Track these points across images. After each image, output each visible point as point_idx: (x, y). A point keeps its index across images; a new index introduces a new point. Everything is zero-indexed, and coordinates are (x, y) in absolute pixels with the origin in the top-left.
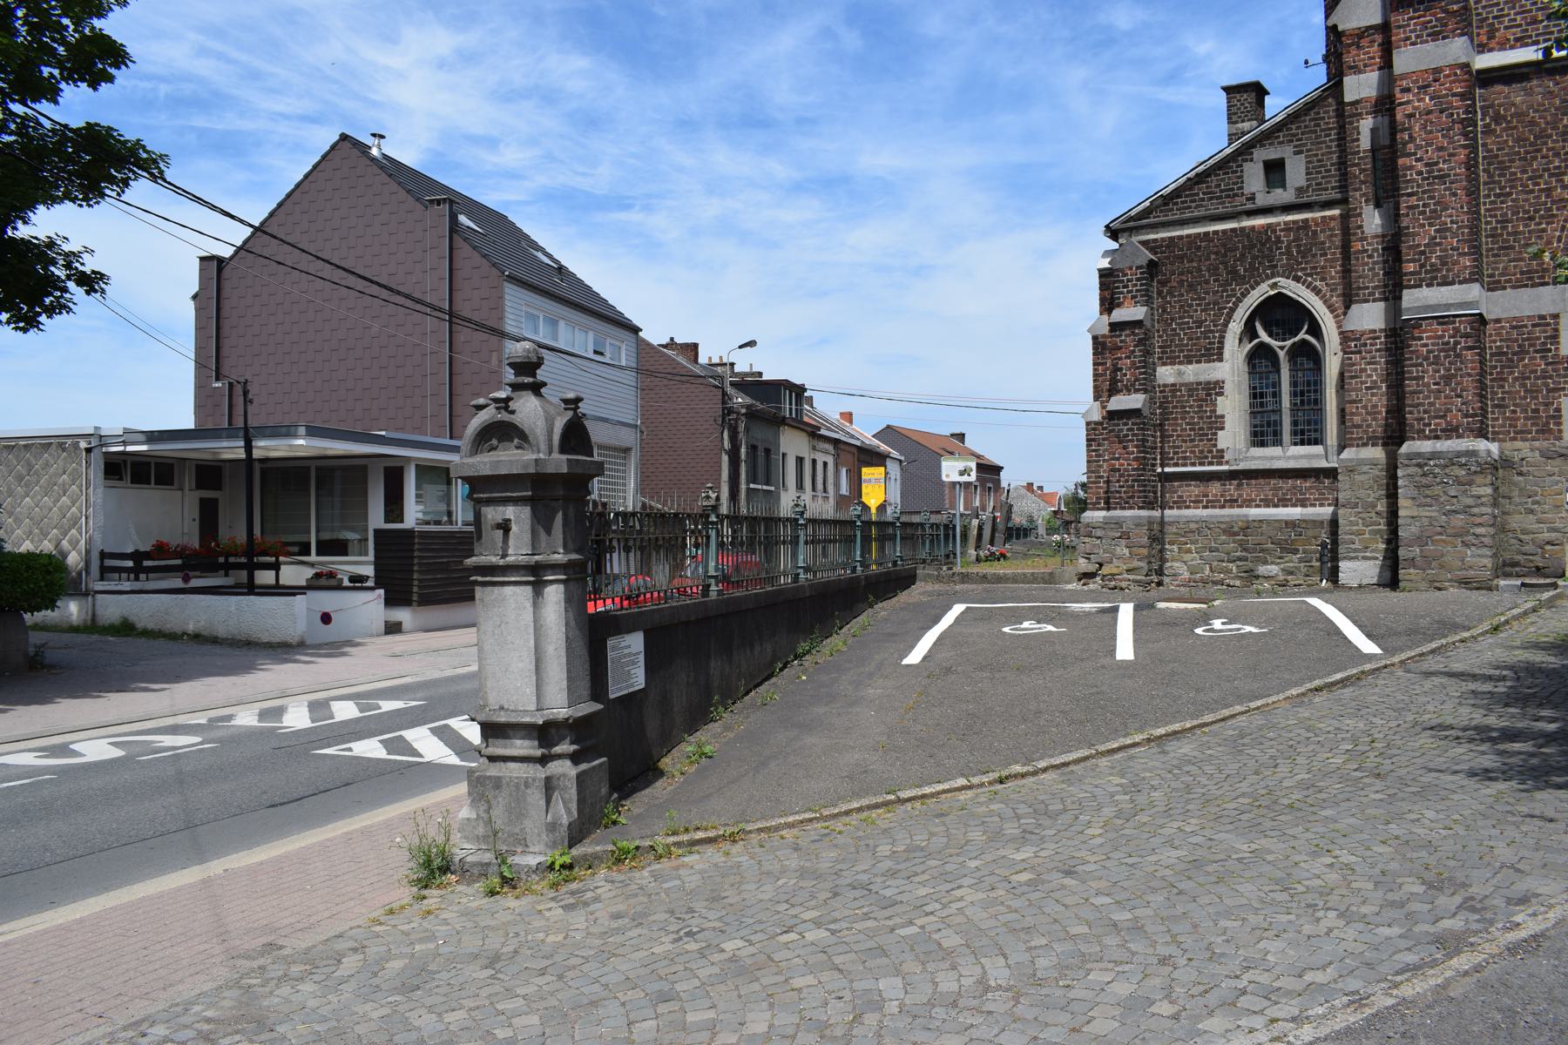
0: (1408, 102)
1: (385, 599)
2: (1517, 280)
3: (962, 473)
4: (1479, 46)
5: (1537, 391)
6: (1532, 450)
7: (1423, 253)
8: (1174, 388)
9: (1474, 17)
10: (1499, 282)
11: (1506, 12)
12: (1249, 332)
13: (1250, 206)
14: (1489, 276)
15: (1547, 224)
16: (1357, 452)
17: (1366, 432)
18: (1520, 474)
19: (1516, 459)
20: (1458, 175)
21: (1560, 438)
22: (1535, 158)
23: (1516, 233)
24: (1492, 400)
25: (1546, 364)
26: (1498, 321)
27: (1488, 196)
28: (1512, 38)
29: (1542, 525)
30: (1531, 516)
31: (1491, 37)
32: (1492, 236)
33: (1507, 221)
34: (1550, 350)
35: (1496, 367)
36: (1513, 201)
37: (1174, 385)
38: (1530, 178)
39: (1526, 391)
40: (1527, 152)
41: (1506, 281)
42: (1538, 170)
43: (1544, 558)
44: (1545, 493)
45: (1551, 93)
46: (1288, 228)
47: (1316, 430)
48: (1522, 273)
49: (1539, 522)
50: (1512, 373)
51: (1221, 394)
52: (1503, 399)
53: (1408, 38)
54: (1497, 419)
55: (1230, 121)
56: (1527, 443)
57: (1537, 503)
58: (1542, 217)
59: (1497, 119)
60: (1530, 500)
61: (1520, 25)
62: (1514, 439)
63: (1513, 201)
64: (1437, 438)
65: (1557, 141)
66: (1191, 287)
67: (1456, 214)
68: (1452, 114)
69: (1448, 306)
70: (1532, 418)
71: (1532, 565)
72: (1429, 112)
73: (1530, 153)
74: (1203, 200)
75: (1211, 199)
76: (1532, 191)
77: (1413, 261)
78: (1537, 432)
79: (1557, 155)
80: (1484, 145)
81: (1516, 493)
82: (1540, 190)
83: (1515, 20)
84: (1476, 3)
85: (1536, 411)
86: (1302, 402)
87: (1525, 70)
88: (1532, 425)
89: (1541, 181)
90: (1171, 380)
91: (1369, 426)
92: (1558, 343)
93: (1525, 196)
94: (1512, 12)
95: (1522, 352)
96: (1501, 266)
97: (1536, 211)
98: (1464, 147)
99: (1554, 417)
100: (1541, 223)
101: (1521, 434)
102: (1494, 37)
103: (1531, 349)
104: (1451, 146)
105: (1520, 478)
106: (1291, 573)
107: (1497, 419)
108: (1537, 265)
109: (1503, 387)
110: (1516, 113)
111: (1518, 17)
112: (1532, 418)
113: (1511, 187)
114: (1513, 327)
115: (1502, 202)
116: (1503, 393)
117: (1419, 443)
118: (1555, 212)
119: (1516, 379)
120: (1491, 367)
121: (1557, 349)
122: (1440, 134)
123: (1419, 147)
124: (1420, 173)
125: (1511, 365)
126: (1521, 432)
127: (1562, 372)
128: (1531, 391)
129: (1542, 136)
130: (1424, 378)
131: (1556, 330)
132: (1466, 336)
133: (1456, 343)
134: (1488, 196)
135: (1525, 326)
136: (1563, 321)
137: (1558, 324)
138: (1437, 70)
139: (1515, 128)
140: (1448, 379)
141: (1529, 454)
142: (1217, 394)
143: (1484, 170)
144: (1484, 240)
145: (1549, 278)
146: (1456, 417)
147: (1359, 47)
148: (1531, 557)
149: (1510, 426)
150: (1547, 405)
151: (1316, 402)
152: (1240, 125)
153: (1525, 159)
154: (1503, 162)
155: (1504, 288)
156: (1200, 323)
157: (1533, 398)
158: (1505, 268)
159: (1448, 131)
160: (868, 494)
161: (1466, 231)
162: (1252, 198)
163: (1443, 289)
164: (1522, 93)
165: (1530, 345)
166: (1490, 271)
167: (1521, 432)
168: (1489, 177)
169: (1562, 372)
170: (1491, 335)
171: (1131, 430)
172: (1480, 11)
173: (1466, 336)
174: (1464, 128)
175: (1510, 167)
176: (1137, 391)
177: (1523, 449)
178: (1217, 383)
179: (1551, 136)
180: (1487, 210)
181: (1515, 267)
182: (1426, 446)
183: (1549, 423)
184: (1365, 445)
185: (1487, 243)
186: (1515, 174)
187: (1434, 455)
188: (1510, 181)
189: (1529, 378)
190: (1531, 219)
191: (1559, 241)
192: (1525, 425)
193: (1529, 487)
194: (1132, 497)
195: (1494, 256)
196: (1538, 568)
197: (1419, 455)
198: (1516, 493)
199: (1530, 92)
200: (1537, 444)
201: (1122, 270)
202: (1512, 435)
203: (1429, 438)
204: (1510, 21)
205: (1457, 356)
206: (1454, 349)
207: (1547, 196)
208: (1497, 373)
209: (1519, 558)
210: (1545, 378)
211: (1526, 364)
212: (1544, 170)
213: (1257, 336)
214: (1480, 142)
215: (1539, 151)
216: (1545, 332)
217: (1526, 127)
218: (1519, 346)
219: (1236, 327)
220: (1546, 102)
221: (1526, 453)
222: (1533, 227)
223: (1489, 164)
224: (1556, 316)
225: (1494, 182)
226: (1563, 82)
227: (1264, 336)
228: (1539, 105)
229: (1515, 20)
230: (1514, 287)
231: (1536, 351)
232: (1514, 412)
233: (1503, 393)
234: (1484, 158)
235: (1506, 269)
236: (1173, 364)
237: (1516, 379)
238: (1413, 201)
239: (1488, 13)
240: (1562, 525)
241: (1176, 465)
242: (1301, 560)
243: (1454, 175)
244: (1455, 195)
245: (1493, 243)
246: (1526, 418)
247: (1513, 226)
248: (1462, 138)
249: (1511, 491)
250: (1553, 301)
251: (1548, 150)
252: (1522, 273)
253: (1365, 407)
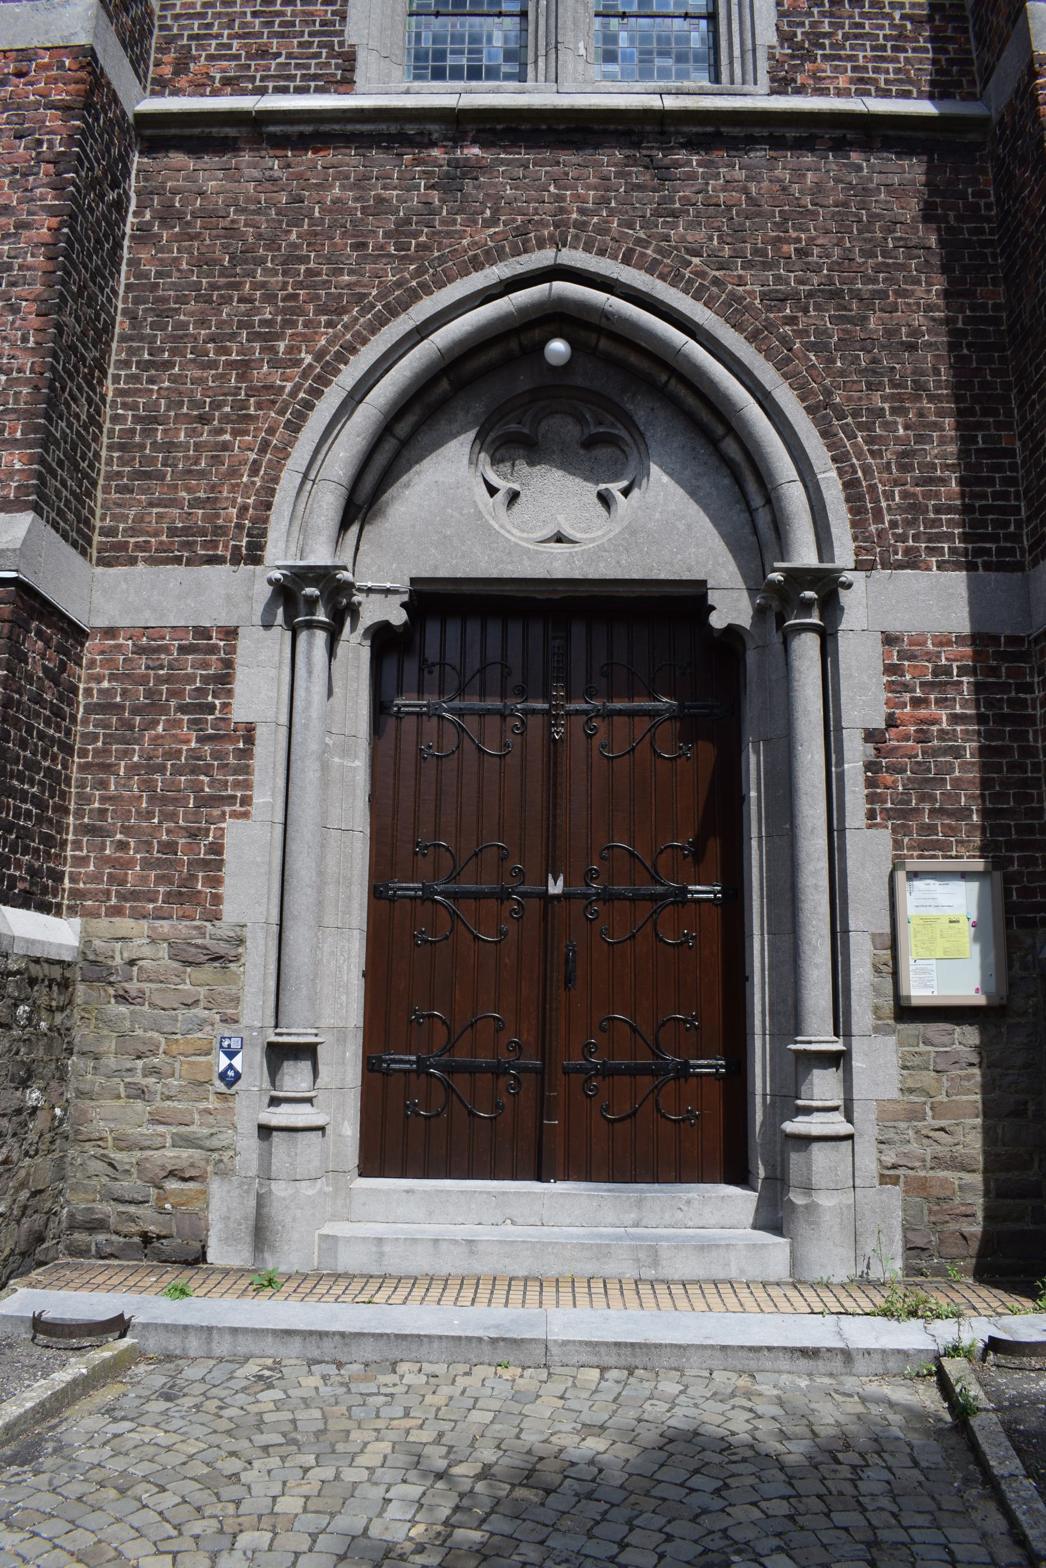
2: (162, 547)
4: (154, 81)
5: (175, 801)
6: (153, 941)
9: (156, 32)
10: (123, 546)
11: (215, 30)
14: (106, 532)
15: (235, 433)
18: (123, 998)
19: (118, 960)
20: (29, 269)
21: (215, 917)
22: (227, 300)
23: (170, 446)
24: (79, 814)
25: (199, 740)
26: (110, 632)
27: (127, 364)
28: (218, 76)
29: (161, 1129)
30: (139, 1104)
31: (181, 67)
32: (122, 447)
33: (155, 420)
34: (211, 709)
35: (95, 737)
36: (173, 379)
38: (212, 339)
39: (151, 799)
40: (213, 287)
41: (138, 546)
42: (229, 323)
43: (161, 1211)
44: (174, 1049)
45: (273, 180)
48: (173, 532)
49: (156, 1120)
50: (127, 754)
52: (103, 812)
54: (83, 861)
56: (144, 924)
57: (153, 1071)
58: (225, 419)
59: (167, 216)
60: (140, 1063)
61: (237, 57)
62: (116, 912)
63: (173, 379)
65: (274, 273)
68: (39, 143)
70: (159, 864)
71: (134, 1228)
73: (218, 288)
76: (213, 365)
78: (168, 898)
79: (270, 298)
80: (133, 263)
81: (110, 1045)
82: (230, 364)
83: (229, 47)
84: (163, 8)
85: (169, 847)
87: (231, 132)
88: (159, 879)
89: (234, 346)
92: (230, 693)
93: (197, 373)
94: (226, 32)
95: (154, 707)
96: (132, 513)
97: (217, 406)
98: (52, 211)
99: (205, 864)
100: (221, 431)
102: (186, 70)
103: (173, 703)
104: (25, 206)
105: (123, 1009)
107: (83, 861)
108: (205, 517)
109: (103, 785)
110: (202, 209)
111: (235, 43)
112: (159, 864)
113: (173, 352)
114: (140, 650)
115: (151, 381)
116: (103, 799)
118: (252, 411)
119: (132, 769)
120: (84, 735)
121: (226, 706)
122: (7, 181)
125: (127, 735)
126: (134, 896)
127: (232, 760)
128: (164, 800)
129: (247, 258)
131: (229, 664)
134: (127, 364)
135: (165, 649)
137: (232, 650)
138: (25, 55)
139: (197, 236)
141: (147, 951)
143: (125, 312)
144: (104, 453)
145: (226, 547)
148: (132, 1209)
149: (112, 878)
150: (194, 834)
153: (209, 301)
154: (165, 300)
155: (132, 561)
157: (166, 816)
158: (140, 519)
159: (25, 175)
161: (25, 390)
164: (220, 174)
165: (172, 694)
166: (108, 521)
167: (134, 896)
168: (133, 327)
169: (232, 760)
170: (92, 664)
172: (169, 22)
174: (58, 174)
175: (177, 311)
179: (262, 261)
180: (120, 392)
181: (160, 517)
183: (193, 877)
185: (109, 462)
186: (185, 326)
188: (174, 338)
189: (162, 769)
190: (203, 419)
191: (254, 471)
192: (144, 879)
193: (139, 1032)
195: (120, 490)
196: (146, 1239)
198: (110, 1045)
199: (232, 174)
202: (114, 901)
204: (221, 46)
207: (241, 378)
208: (96, 751)
209: (107, 1209)
210: (195, 770)
211: (158, 737)
212: (241, 325)
214: (126, 254)
215: (237, 286)
216: (206, 665)
217: (218, 237)
218: (149, 694)
220: (263, 197)
221: (139, 947)
222: (204, 437)
223: (137, 301)
225: (142, 338)
226: (299, 164)
228: (248, 200)
229: (229, 47)
230: (152, 561)
231: (183, 709)
232: (123, 846)
233: (103, 799)
234: (128, 287)
235: (142, 520)
237: (132, 769)
239: (182, 28)
240: (206, 1131)
243: (21, 267)
244: (15, 310)
245: (122, 462)
246: (147, 864)
247: (165, 431)
248: (50, 193)
249: (100, 1039)
250: (228, 597)
251: (255, 287)
252: (173, 532)
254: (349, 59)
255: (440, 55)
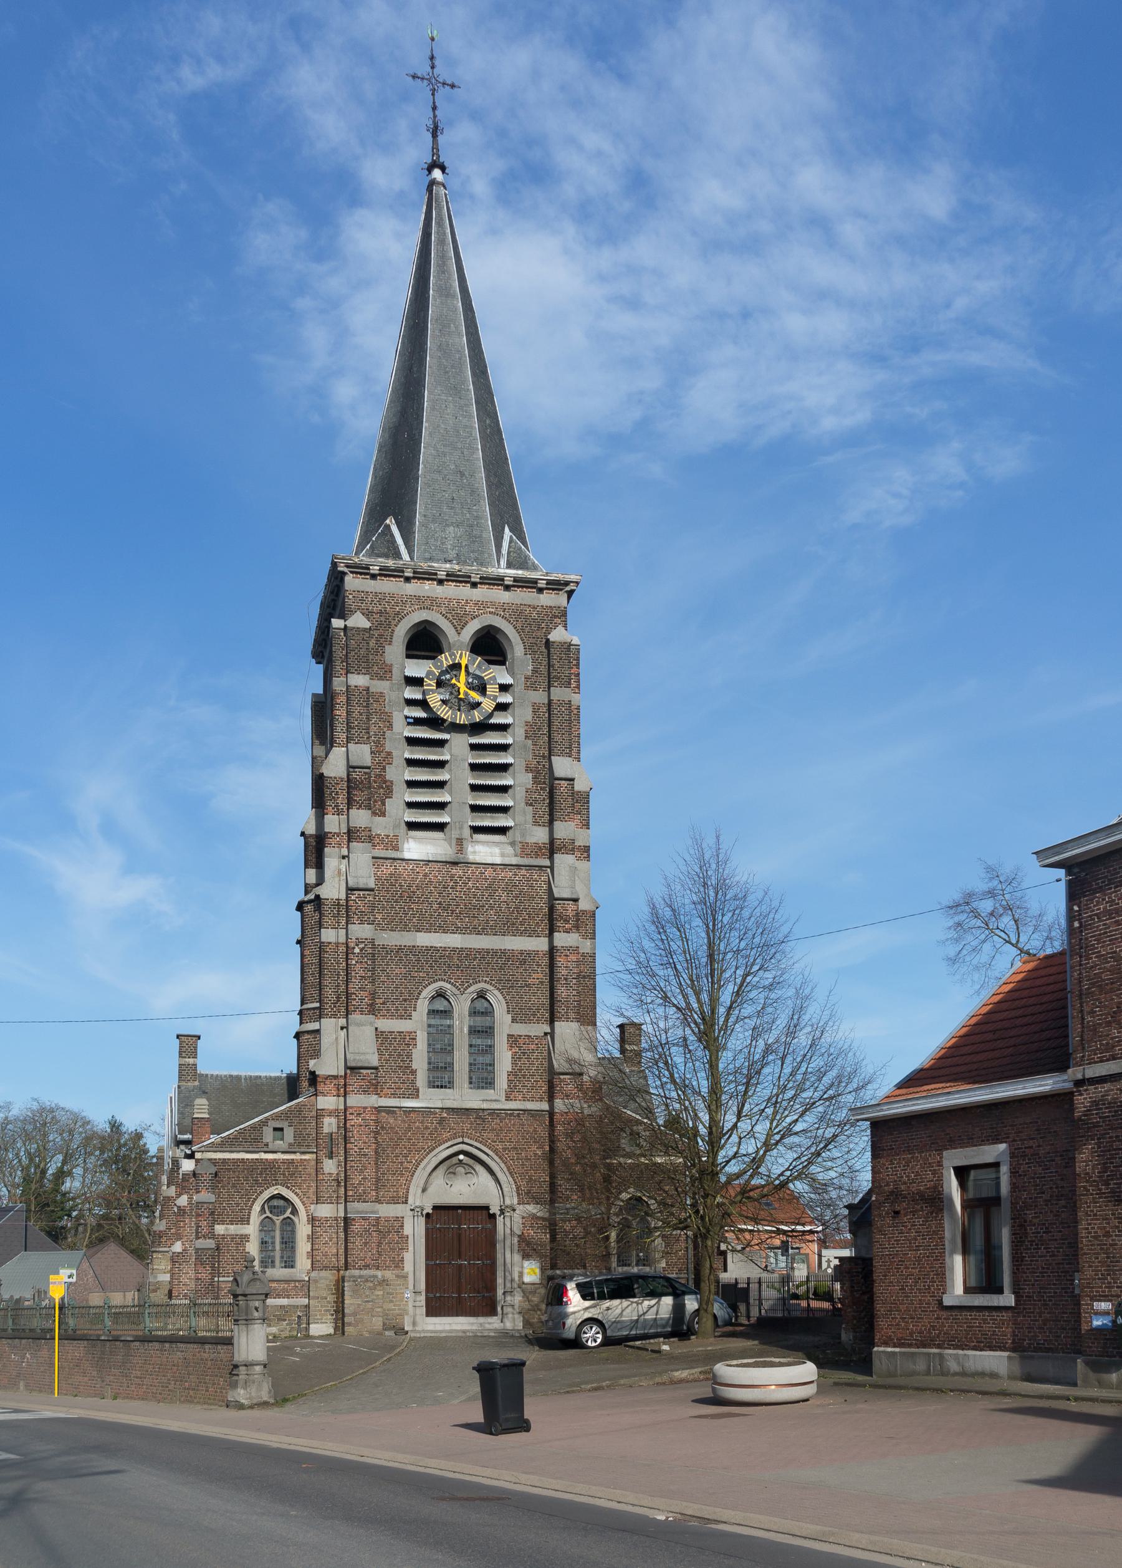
0: (352, 1119)
1: (428, 1300)
3: (69, 1277)
7: (356, 1187)
8: (224, 1237)
12: (263, 1210)
13: (266, 1149)
16: (319, 1273)
17: (322, 1264)
37: (224, 1235)
46: (284, 1162)
47: (292, 1261)
51: (249, 1241)
53: (354, 1091)
55: (180, 1056)
62: (385, 1269)
64: (361, 1269)
66: (234, 1186)
67: (370, 1172)
69: (367, 1213)
72: (361, 1126)
74: (242, 1142)
75: (246, 1142)
77: (352, 1190)
86: (286, 1247)
90: (222, 1233)
91: (324, 1261)
98: (375, 1143)
101: (388, 1268)
106: (282, 1331)
117: (353, 1271)
119: (386, 1243)
123: (356, 1140)
124: (356, 1152)
130: (357, 1243)
132: (374, 1225)
133: (370, 1228)
136: (405, 1219)
138: (365, 1108)
140: (366, 1244)
142: (246, 1241)
146: (368, 1261)
147: (325, 1084)
150: (399, 1255)
151: (292, 1247)
152: (187, 1060)
156: (238, 1205)
160: (53, 1291)
162: (267, 1145)
163: (364, 1204)
171: (209, 1258)
173: (374, 1225)
176: (209, 1238)
177: (389, 1274)
178: (246, 1235)
182: (357, 1272)
184: (321, 1270)
187: (360, 1277)
194: (208, 1293)
197: (354, 1277)
200: (394, 1272)
201: (201, 1174)
203: (357, 1269)
205: (370, 1234)
206: (369, 1231)
213: (265, 1213)
219: (257, 1208)
224: (403, 1217)
227: (268, 1214)
236: (224, 1224)
237: (386, 1243)
238: (353, 1164)
241: (224, 1276)
242: (287, 1324)
253: (322, 1252)
254: (418, 1090)
255: (434, 1082)
